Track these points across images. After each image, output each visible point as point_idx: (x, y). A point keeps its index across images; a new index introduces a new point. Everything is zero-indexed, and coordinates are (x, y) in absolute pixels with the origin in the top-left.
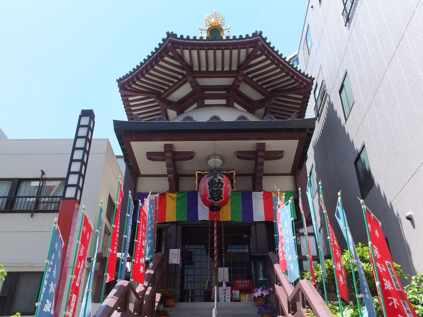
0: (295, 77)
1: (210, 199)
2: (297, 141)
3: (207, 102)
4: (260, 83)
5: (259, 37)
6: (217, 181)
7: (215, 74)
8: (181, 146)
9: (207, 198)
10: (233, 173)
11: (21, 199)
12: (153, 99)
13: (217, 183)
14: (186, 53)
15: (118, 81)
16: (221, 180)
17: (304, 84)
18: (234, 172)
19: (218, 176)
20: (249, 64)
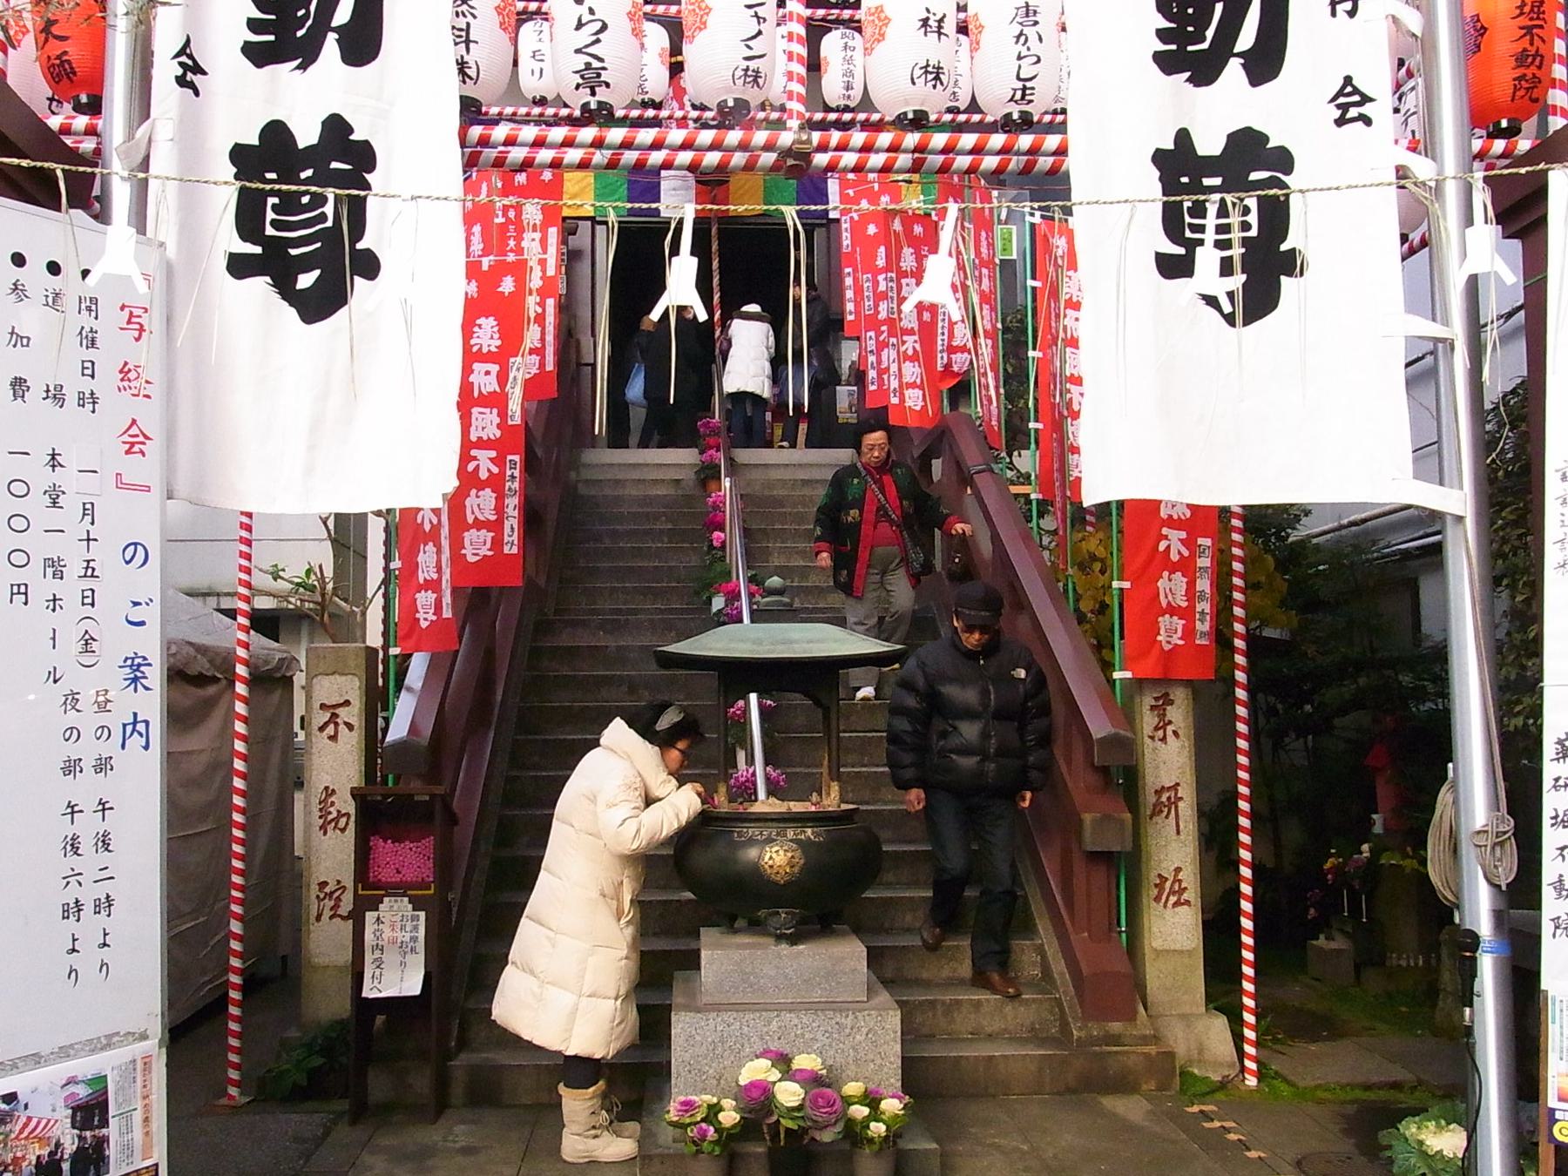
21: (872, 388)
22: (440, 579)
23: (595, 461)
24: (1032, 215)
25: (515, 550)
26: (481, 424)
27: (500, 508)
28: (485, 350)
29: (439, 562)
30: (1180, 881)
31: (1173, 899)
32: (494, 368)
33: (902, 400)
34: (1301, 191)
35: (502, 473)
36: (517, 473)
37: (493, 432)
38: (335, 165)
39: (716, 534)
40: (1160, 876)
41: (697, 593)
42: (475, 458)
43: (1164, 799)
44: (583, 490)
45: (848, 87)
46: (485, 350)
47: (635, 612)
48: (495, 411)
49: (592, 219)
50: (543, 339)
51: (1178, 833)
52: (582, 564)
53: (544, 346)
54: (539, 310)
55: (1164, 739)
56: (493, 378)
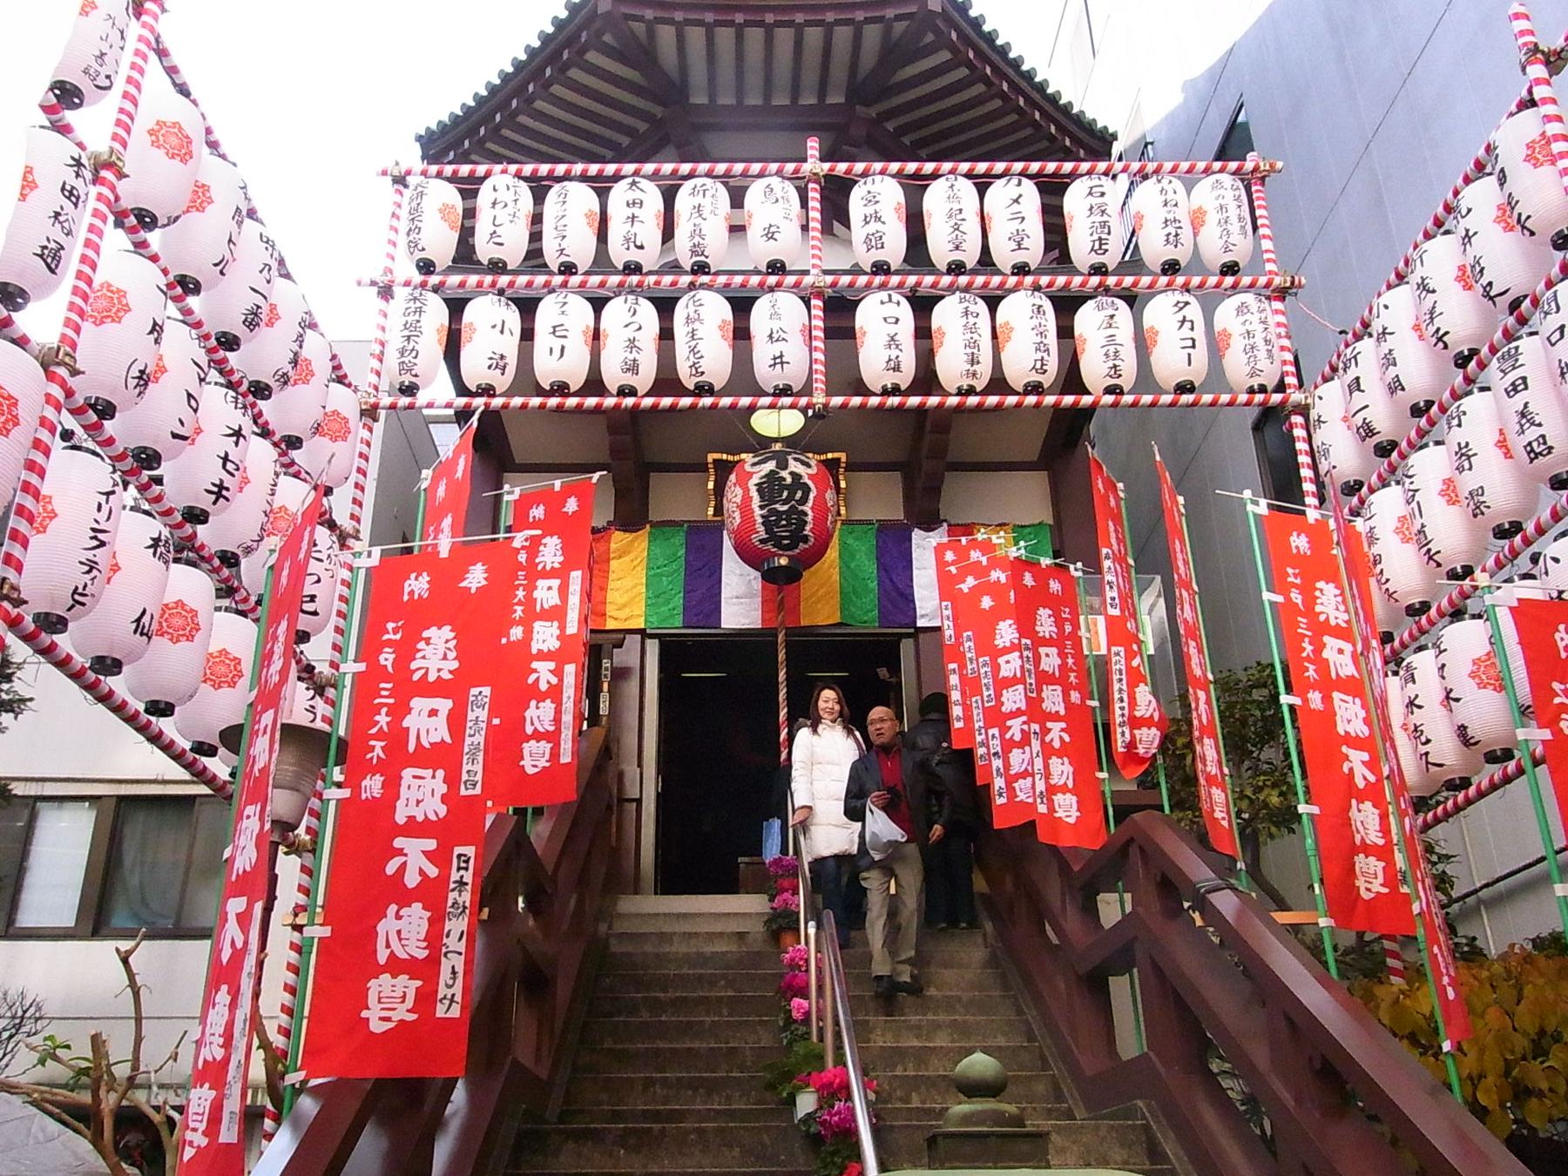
1: (762, 541)
6: (789, 480)
9: (755, 538)
13: (787, 487)
14: (666, 34)
15: (419, 138)
16: (800, 477)
19: (791, 462)
20: (892, 81)
21: (1000, 801)
22: (226, 1060)
23: (633, 910)
24: (1256, 503)
25: (455, 1012)
26: (414, 795)
27: (434, 939)
28: (432, 678)
29: (230, 1026)
32: (444, 705)
33: (1052, 809)
35: (444, 878)
36: (468, 877)
37: (434, 808)
39: (797, 1001)
41: (771, 1087)
42: (400, 852)
44: (616, 947)
45: (973, 361)
46: (432, 678)
47: (678, 1116)
48: (440, 773)
49: (642, 632)
50: (557, 720)
52: (608, 1044)
53: (558, 731)
54: (554, 680)
56: (441, 722)
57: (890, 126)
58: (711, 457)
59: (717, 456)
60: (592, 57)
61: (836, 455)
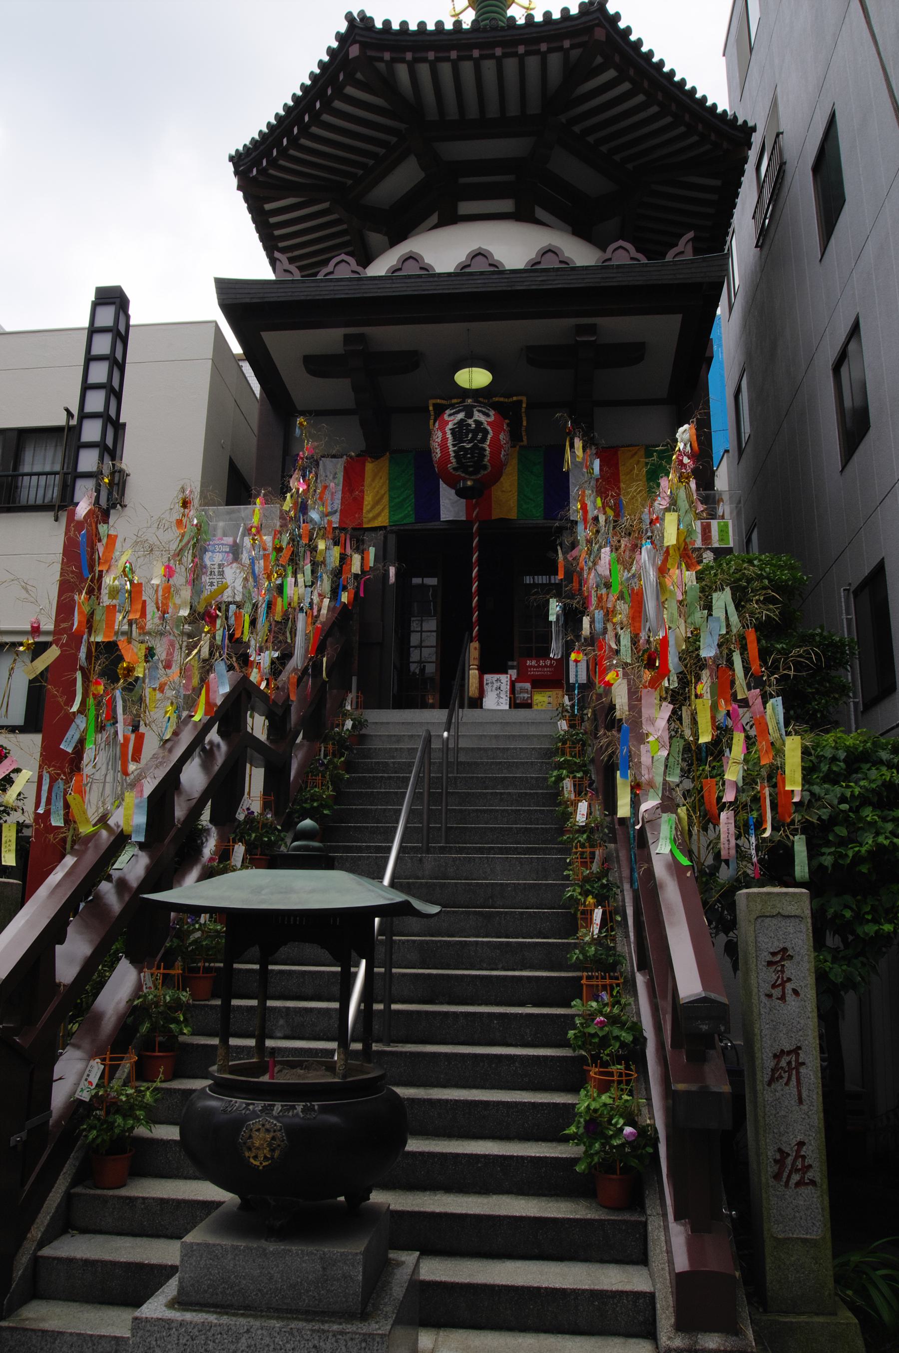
0: (700, 127)
1: (454, 469)
2: (679, 317)
3: (465, 208)
4: (604, 149)
5: (598, 14)
7: (484, 127)
8: (390, 336)
10: (520, 402)
11: (26, 478)
12: (326, 205)
13: (472, 431)
14: (402, 71)
15: (231, 159)
17: (725, 145)
18: (524, 399)
30: (804, 1157)
31: (796, 1177)
34: (12, 668)
38: (377, 920)
40: (780, 1150)
43: (783, 1063)
51: (800, 1101)
55: (783, 998)
57: (577, 129)
58: (431, 402)
59: (434, 401)
60: (350, 90)
61: (520, 398)
